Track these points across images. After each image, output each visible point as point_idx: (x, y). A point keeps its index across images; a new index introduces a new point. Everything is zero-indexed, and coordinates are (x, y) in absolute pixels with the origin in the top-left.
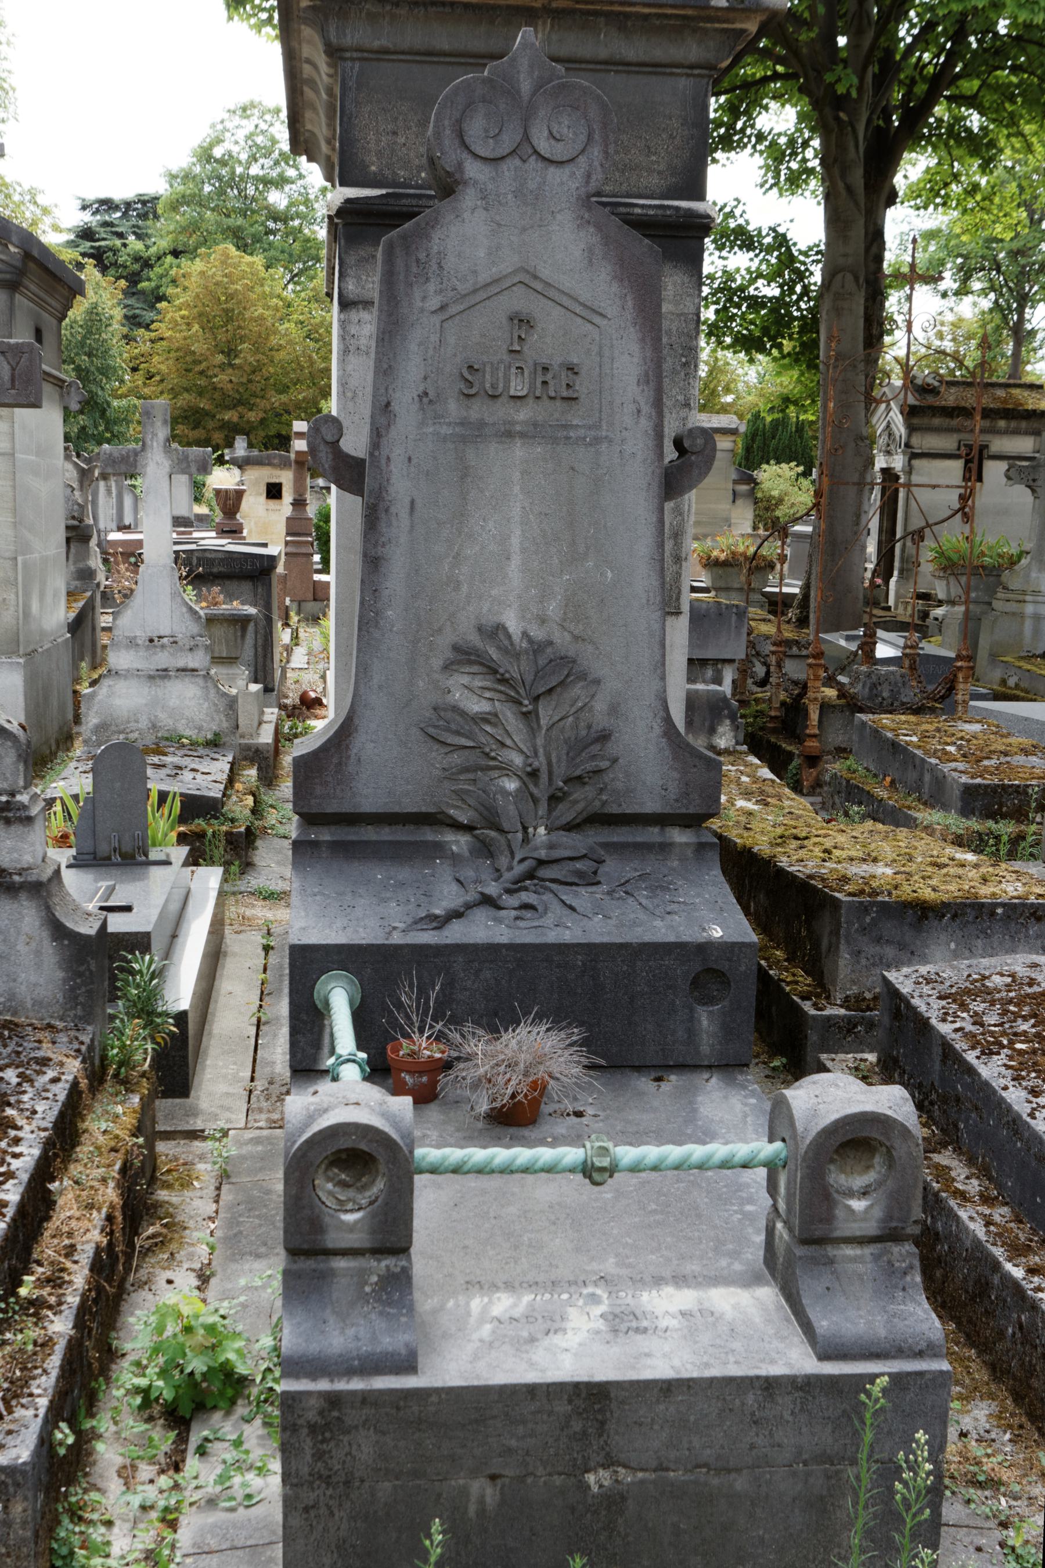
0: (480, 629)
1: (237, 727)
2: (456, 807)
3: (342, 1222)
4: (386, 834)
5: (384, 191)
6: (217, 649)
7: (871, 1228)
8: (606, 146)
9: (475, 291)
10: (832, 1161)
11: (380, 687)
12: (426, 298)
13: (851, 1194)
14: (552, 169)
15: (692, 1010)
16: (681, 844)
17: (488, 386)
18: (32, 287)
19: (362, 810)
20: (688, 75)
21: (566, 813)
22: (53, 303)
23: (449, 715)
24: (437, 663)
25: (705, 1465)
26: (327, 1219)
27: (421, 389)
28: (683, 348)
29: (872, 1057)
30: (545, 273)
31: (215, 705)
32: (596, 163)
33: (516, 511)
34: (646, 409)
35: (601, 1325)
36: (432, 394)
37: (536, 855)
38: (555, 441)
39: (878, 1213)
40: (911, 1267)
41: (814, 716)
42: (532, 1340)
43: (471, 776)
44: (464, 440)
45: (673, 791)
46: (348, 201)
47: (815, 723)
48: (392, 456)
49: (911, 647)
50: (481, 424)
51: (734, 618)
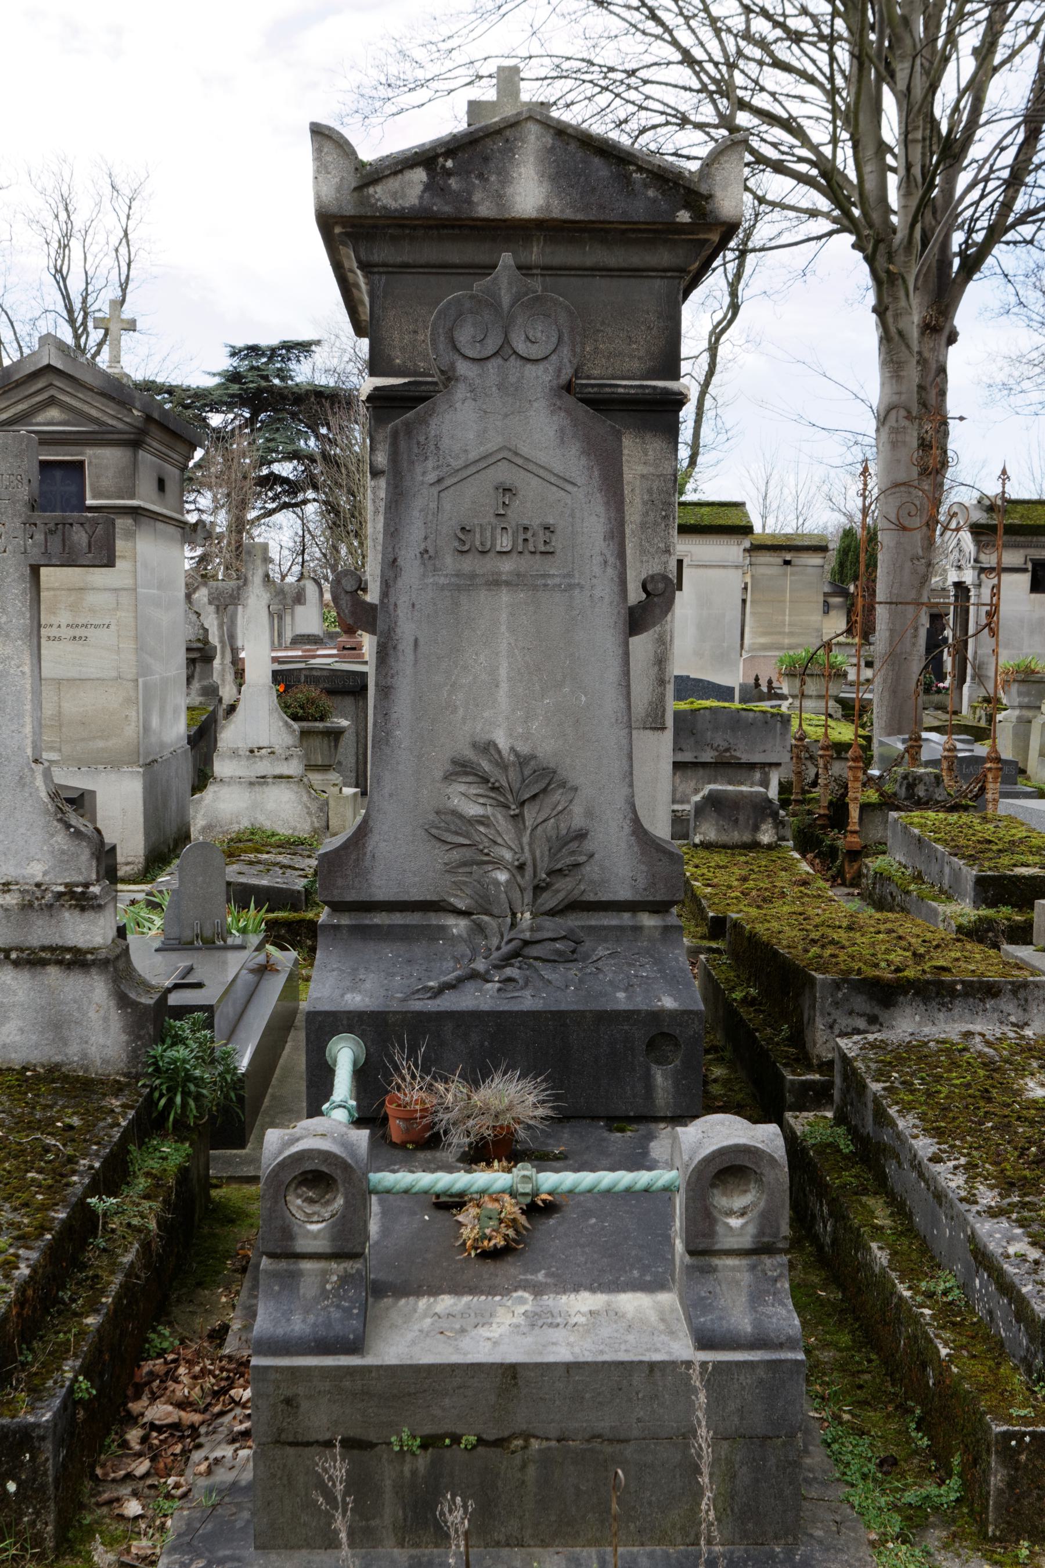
0: (474, 745)
1: (328, 828)
2: (456, 896)
3: (308, 1231)
4: (398, 919)
5: (406, 380)
6: (312, 757)
7: (746, 1242)
8: (574, 346)
9: (466, 467)
10: (713, 1185)
11: (391, 795)
12: (425, 473)
13: (730, 1213)
14: (529, 366)
15: (648, 1069)
16: (649, 927)
17: (478, 543)
18: (155, 444)
19: (376, 899)
20: (662, 277)
21: (549, 900)
22: (175, 456)
23: (449, 818)
24: (439, 774)
25: (599, 1436)
26: (296, 1229)
27: (422, 547)
28: (663, 504)
29: (829, 1115)
30: (524, 450)
31: (308, 808)
32: (566, 360)
33: (503, 647)
34: (611, 560)
35: (520, 1320)
36: (431, 552)
37: (521, 936)
38: (535, 588)
39: (751, 1229)
40: (780, 1276)
41: (854, 813)
42: (463, 1330)
43: (467, 869)
44: (459, 588)
45: (642, 882)
46: (376, 389)
47: (856, 820)
48: (399, 603)
49: (949, 750)
50: (473, 576)
51: (779, 725)
